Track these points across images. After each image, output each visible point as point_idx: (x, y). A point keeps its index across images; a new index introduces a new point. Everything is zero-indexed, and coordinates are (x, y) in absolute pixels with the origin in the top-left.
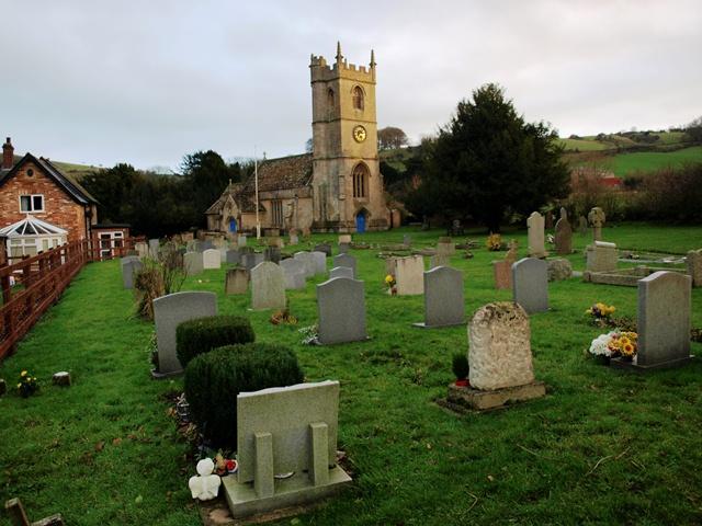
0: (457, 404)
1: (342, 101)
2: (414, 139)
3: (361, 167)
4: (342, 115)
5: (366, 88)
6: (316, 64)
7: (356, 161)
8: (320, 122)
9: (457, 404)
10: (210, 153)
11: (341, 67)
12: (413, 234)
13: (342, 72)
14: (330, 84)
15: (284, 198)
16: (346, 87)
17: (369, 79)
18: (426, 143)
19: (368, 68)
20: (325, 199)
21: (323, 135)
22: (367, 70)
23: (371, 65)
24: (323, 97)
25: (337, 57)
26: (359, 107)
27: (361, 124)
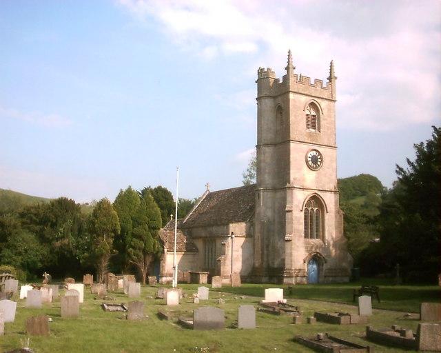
0: (161, 316)
1: (292, 118)
2: (388, 180)
3: (316, 200)
4: (293, 136)
5: (323, 104)
6: (263, 76)
7: (309, 194)
8: (266, 145)
9: (161, 316)
10: (159, 188)
11: (292, 80)
12: (362, 248)
13: (293, 85)
14: (279, 100)
15: (218, 237)
16: (298, 104)
17: (326, 94)
18: (405, 181)
19: (326, 81)
20: (268, 239)
21: (268, 160)
22: (325, 85)
23: (330, 79)
24: (269, 116)
25: (287, 68)
26: (314, 127)
27: (316, 147)
